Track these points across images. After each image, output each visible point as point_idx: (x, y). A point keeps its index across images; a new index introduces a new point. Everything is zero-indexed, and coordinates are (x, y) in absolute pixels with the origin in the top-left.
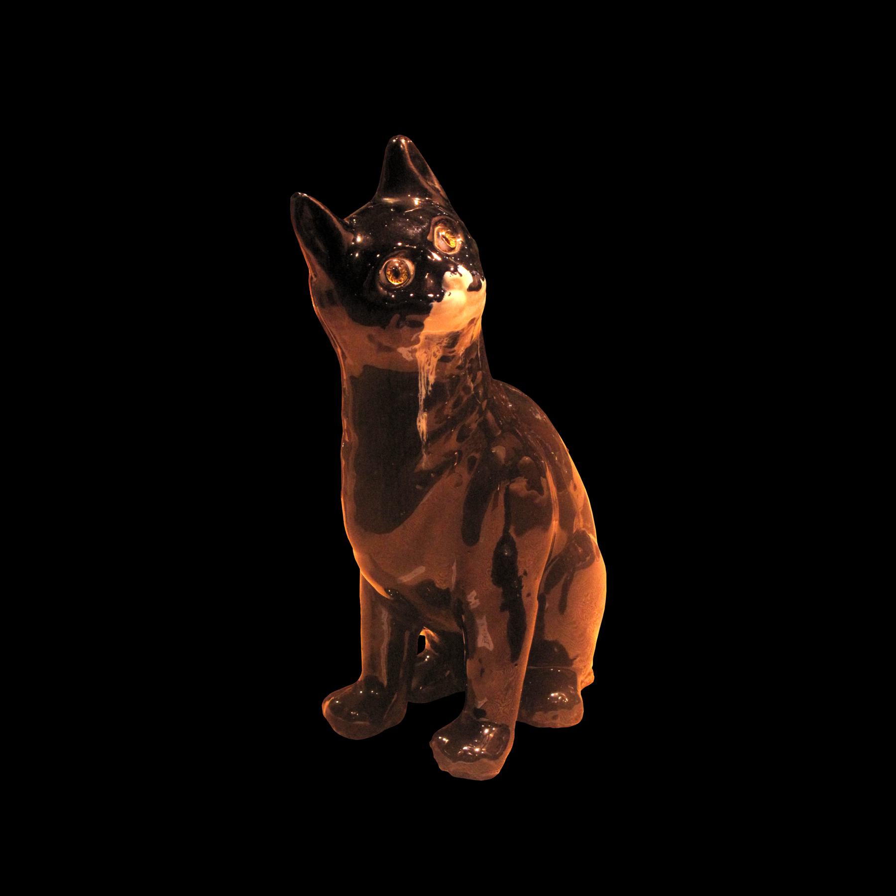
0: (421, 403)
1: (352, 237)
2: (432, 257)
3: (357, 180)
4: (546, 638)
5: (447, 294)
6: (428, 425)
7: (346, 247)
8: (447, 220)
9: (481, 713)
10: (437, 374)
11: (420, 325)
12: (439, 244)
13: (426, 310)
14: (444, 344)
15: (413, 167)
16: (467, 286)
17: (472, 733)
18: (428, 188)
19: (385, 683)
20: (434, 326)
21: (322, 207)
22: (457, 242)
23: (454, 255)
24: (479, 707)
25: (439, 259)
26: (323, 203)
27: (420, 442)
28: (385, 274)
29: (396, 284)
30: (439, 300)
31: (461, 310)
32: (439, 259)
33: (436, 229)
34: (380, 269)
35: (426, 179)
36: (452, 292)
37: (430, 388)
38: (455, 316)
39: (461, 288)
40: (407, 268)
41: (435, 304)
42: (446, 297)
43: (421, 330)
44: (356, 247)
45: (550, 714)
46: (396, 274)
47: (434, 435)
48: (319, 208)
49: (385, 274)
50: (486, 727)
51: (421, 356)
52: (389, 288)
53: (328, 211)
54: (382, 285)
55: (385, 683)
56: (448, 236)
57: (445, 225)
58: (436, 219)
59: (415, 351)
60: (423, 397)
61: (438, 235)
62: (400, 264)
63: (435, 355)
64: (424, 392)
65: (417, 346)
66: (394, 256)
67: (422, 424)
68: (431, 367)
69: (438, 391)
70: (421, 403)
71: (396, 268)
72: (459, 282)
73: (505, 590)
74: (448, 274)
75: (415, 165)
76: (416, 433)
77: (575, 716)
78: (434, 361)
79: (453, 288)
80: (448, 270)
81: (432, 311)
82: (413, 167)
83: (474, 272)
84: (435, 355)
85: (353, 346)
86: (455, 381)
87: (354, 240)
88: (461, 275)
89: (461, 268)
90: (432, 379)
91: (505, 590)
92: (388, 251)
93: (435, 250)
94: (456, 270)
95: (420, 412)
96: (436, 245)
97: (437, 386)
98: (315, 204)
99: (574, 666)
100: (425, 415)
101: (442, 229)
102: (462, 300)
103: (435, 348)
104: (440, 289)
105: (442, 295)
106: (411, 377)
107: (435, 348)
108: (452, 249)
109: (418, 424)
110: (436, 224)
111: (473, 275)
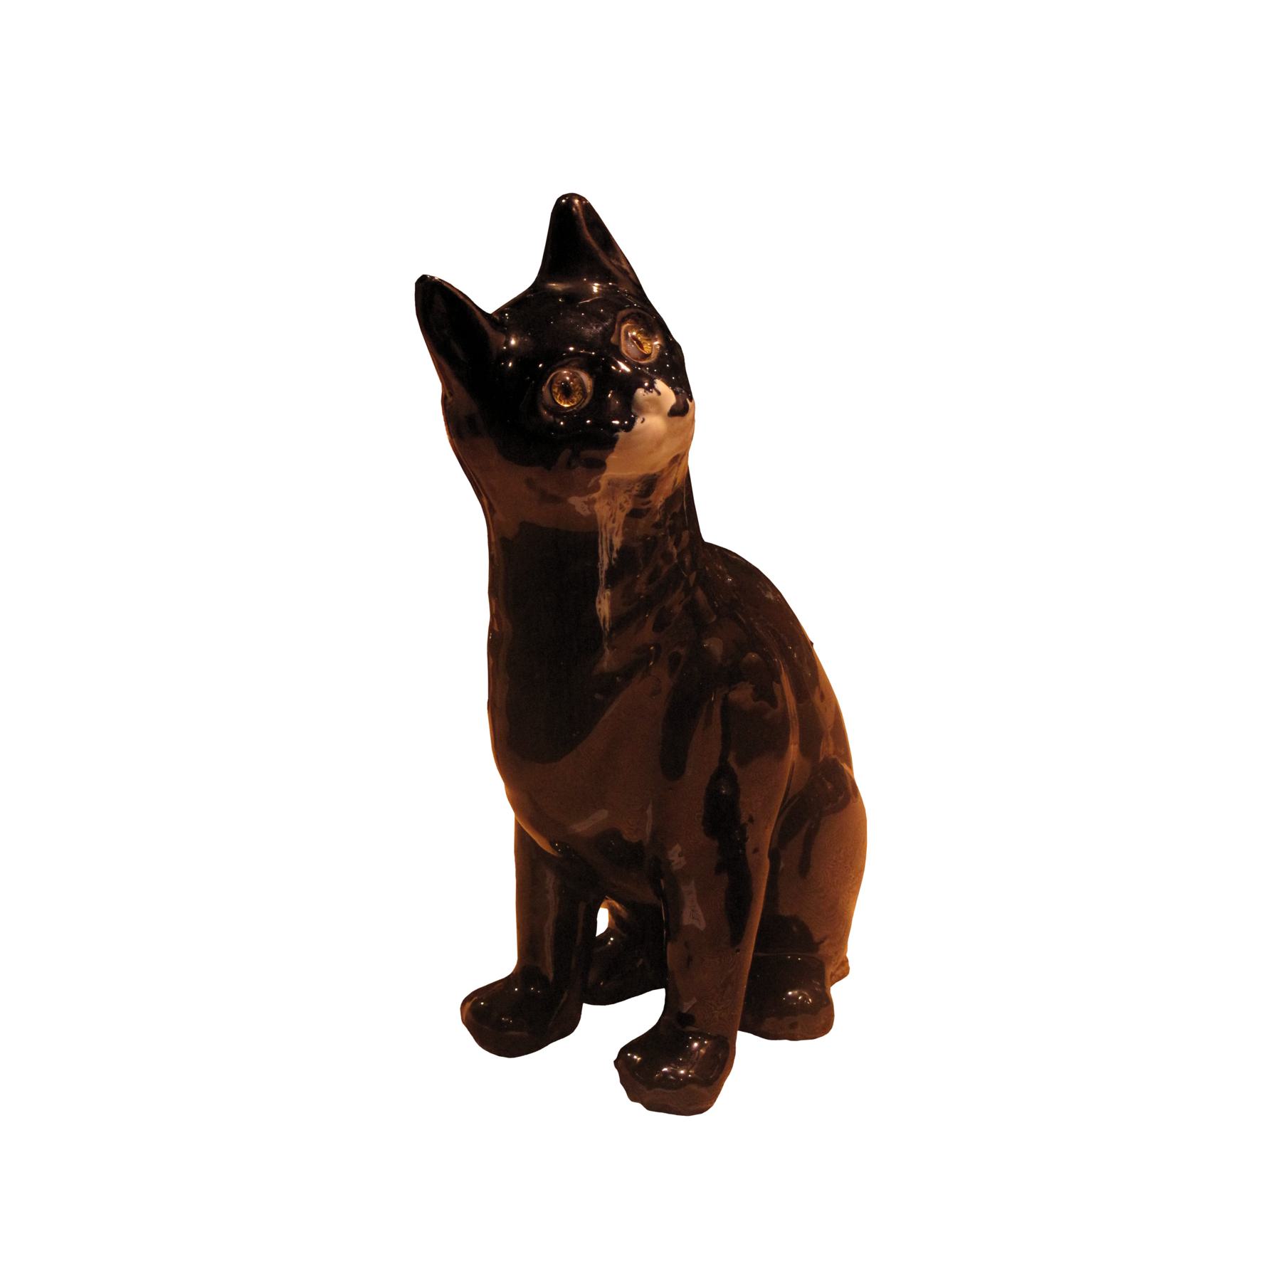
0: (602, 576)
2: (618, 367)
5: (639, 421)
6: (612, 607)
8: (639, 314)
10: (624, 535)
11: (600, 465)
12: (627, 348)
13: (609, 442)
14: (634, 492)
15: (590, 239)
16: (668, 408)
18: (612, 268)
20: (621, 467)
23: (649, 365)
25: (628, 370)
28: (551, 392)
30: (628, 428)
31: (659, 443)
32: (628, 370)
33: (624, 327)
34: (544, 384)
35: (608, 256)
37: (615, 555)
38: (651, 452)
39: (659, 411)
40: (581, 383)
41: (621, 434)
43: (602, 472)
44: (510, 353)
46: (567, 392)
47: (620, 622)
49: (551, 392)
51: (602, 510)
52: (557, 411)
54: (546, 408)
57: (636, 321)
58: (624, 313)
59: (594, 501)
60: (605, 567)
63: (621, 507)
64: (606, 560)
65: (596, 495)
66: (563, 367)
67: (604, 607)
68: (616, 525)
69: (626, 560)
70: (602, 576)
71: (566, 382)
72: (656, 404)
74: (640, 391)
75: (593, 236)
76: (596, 619)
78: (621, 516)
79: (648, 412)
80: (641, 386)
81: (618, 444)
82: (590, 239)
83: (678, 389)
84: (621, 507)
87: (507, 343)
88: (659, 393)
89: (660, 384)
90: (617, 542)
92: (555, 359)
93: (623, 359)
94: (652, 386)
95: (601, 588)
96: (623, 350)
97: (625, 551)
100: (608, 593)
101: (631, 329)
103: (621, 498)
104: (629, 412)
105: (632, 422)
106: (587, 539)
107: (621, 498)
108: (648, 356)
109: (598, 606)
110: (623, 321)
111: (676, 393)
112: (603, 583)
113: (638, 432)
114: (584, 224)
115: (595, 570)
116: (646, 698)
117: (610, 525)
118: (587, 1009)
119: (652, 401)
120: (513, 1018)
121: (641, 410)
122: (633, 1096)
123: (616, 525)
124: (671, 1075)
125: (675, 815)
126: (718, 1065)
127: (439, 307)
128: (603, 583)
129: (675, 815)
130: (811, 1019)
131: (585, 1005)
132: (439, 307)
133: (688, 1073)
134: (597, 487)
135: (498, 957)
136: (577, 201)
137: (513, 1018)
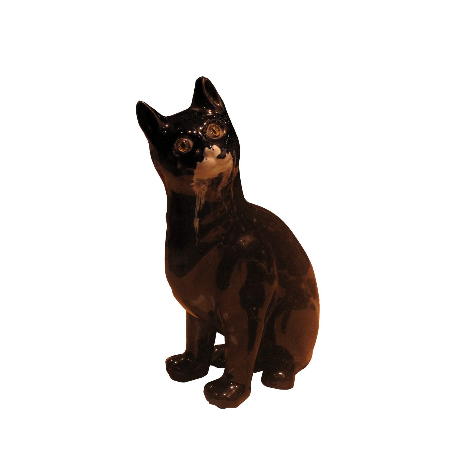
0: (196, 213)
1: (164, 124)
5: (205, 159)
11: (192, 174)
16: (217, 155)
19: (196, 356)
20: (198, 175)
30: (201, 160)
31: (213, 167)
37: (202, 206)
41: (198, 163)
42: (205, 160)
44: (166, 129)
46: (183, 146)
50: (233, 385)
51: (196, 190)
52: (179, 152)
55: (196, 356)
56: (216, 130)
60: (198, 210)
62: (186, 141)
64: (198, 207)
65: (193, 184)
67: (196, 224)
69: (207, 208)
70: (196, 213)
71: (183, 143)
72: (212, 154)
76: (193, 228)
78: (204, 193)
81: (197, 166)
84: (203, 189)
87: (165, 126)
88: (213, 150)
90: (203, 202)
96: (207, 133)
97: (206, 204)
101: (213, 126)
106: (193, 198)
109: (194, 224)
111: (222, 151)
112: (196, 215)
114: (204, 87)
117: (200, 195)
118: (211, 366)
119: (209, 152)
120: (181, 369)
121: (207, 155)
122: (211, 403)
124: (226, 394)
125: (244, 299)
126: (243, 392)
127: (145, 114)
128: (196, 215)
129: (244, 299)
130: (281, 375)
131: (211, 366)
132: (145, 114)
133: (227, 395)
134: (193, 182)
135: (179, 347)
136: (204, 80)
137: (181, 369)
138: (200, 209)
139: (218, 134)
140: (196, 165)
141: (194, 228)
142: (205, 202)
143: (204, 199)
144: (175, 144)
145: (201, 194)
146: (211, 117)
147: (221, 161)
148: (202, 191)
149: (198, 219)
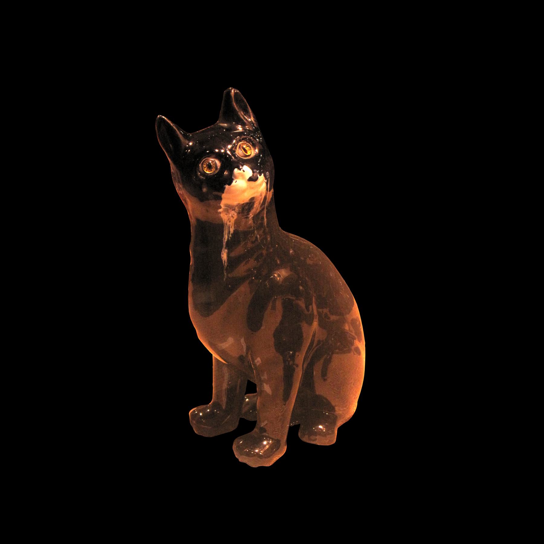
0: (224, 244)
1: (187, 142)
3: (205, 114)
4: (317, 393)
5: (234, 181)
7: (183, 148)
9: (263, 430)
11: (220, 199)
16: (248, 178)
17: (257, 442)
20: (227, 199)
21: (172, 125)
22: (253, 152)
24: (262, 426)
26: (173, 122)
27: (223, 266)
29: (207, 172)
30: (230, 184)
31: (244, 191)
35: (253, 203)
36: (237, 180)
37: (230, 236)
41: (227, 186)
42: (234, 183)
44: (190, 147)
45: (313, 437)
46: (209, 167)
48: (169, 124)
50: (266, 440)
51: (224, 217)
52: (204, 174)
53: (174, 127)
55: (224, 407)
56: (247, 149)
60: (226, 240)
61: (240, 147)
65: (220, 210)
67: (224, 256)
69: (237, 238)
70: (224, 244)
71: (209, 163)
72: (243, 177)
73: (292, 360)
74: (236, 170)
77: (331, 439)
78: (233, 220)
81: (226, 190)
84: (232, 216)
85: (193, 207)
86: (247, 234)
87: (188, 144)
88: (244, 171)
90: (232, 230)
91: (292, 360)
96: (237, 152)
97: (236, 233)
98: (168, 123)
99: (336, 412)
102: (248, 186)
106: (220, 227)
109: (222, 256)
111: (253, 172)
113: (234, 186)
115: (221, 241)
116: (243, 294)
117: (228, 223)
119: (239, 173)
121: (236, 178)
123: (231, 223)
133: (259, 451)
134: (220, 208)
138: (228, 239)
139: (249, 153)
140: (225, 188)
141: (222, 261)
142: (234, 231)
143: (233, 227)
144: (200, 165)
145: (230, 222)
146: (240, 134)
147: (252, 183)
148: (231, 218)
149: (226, 251)
